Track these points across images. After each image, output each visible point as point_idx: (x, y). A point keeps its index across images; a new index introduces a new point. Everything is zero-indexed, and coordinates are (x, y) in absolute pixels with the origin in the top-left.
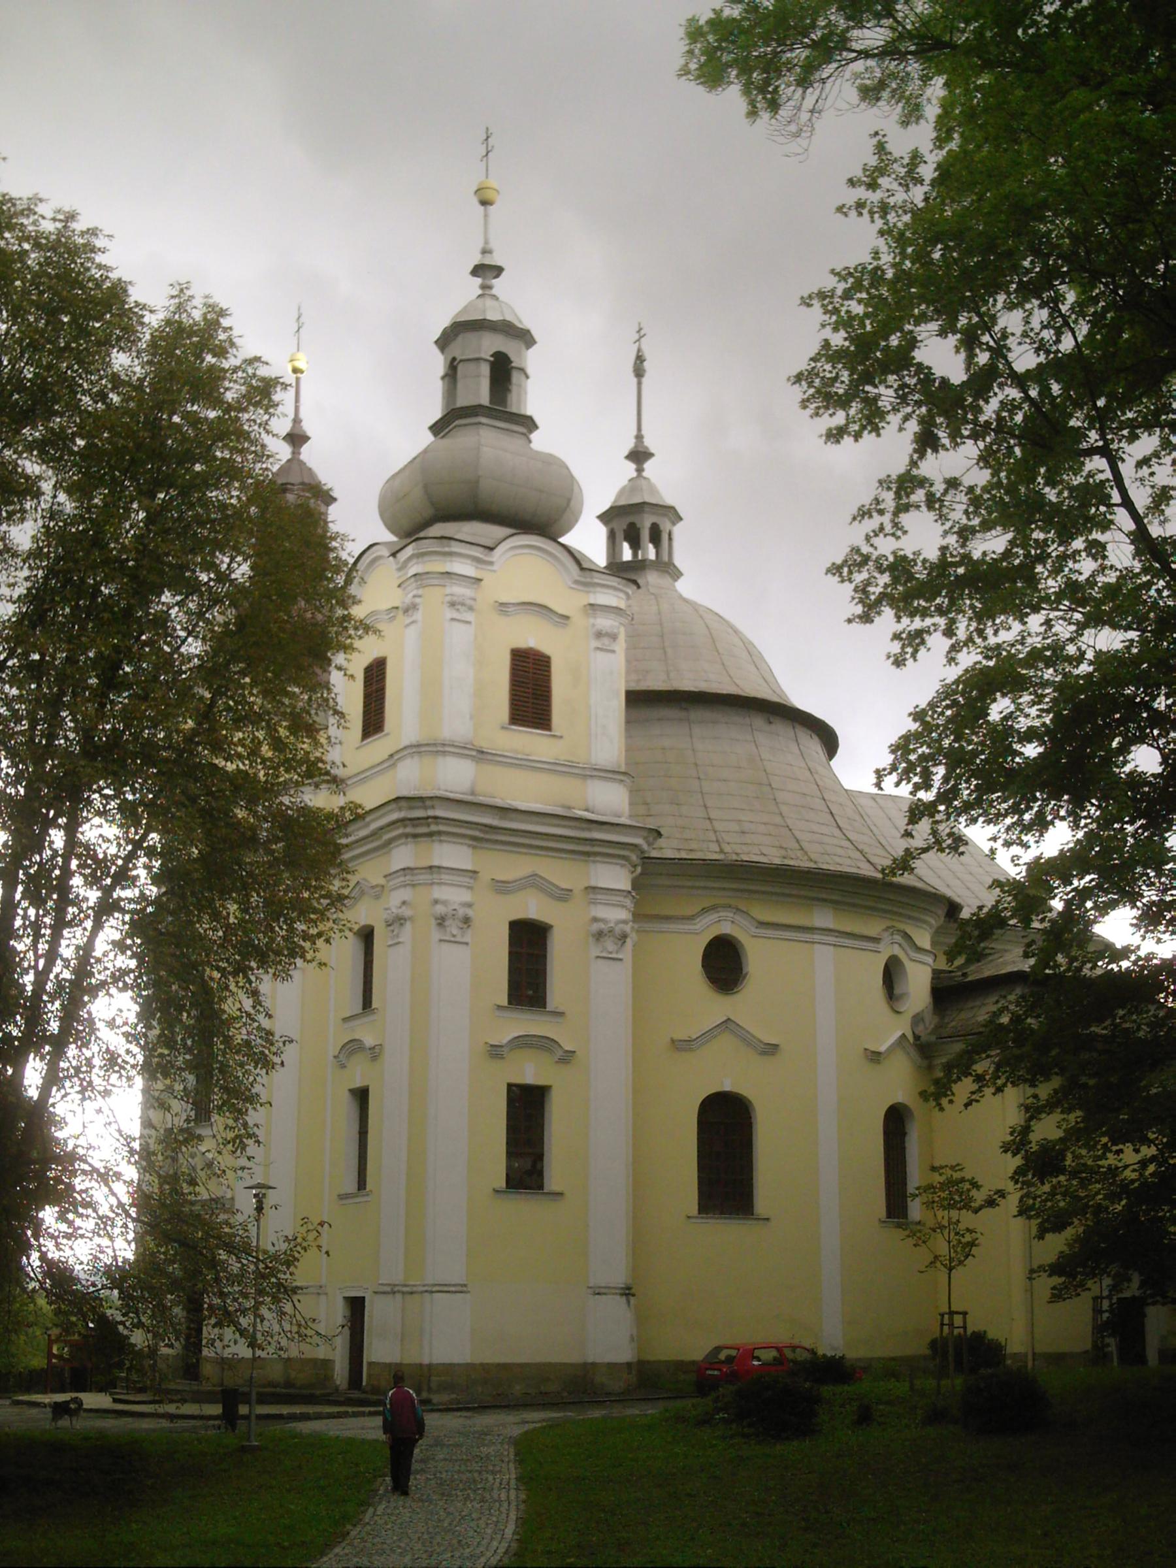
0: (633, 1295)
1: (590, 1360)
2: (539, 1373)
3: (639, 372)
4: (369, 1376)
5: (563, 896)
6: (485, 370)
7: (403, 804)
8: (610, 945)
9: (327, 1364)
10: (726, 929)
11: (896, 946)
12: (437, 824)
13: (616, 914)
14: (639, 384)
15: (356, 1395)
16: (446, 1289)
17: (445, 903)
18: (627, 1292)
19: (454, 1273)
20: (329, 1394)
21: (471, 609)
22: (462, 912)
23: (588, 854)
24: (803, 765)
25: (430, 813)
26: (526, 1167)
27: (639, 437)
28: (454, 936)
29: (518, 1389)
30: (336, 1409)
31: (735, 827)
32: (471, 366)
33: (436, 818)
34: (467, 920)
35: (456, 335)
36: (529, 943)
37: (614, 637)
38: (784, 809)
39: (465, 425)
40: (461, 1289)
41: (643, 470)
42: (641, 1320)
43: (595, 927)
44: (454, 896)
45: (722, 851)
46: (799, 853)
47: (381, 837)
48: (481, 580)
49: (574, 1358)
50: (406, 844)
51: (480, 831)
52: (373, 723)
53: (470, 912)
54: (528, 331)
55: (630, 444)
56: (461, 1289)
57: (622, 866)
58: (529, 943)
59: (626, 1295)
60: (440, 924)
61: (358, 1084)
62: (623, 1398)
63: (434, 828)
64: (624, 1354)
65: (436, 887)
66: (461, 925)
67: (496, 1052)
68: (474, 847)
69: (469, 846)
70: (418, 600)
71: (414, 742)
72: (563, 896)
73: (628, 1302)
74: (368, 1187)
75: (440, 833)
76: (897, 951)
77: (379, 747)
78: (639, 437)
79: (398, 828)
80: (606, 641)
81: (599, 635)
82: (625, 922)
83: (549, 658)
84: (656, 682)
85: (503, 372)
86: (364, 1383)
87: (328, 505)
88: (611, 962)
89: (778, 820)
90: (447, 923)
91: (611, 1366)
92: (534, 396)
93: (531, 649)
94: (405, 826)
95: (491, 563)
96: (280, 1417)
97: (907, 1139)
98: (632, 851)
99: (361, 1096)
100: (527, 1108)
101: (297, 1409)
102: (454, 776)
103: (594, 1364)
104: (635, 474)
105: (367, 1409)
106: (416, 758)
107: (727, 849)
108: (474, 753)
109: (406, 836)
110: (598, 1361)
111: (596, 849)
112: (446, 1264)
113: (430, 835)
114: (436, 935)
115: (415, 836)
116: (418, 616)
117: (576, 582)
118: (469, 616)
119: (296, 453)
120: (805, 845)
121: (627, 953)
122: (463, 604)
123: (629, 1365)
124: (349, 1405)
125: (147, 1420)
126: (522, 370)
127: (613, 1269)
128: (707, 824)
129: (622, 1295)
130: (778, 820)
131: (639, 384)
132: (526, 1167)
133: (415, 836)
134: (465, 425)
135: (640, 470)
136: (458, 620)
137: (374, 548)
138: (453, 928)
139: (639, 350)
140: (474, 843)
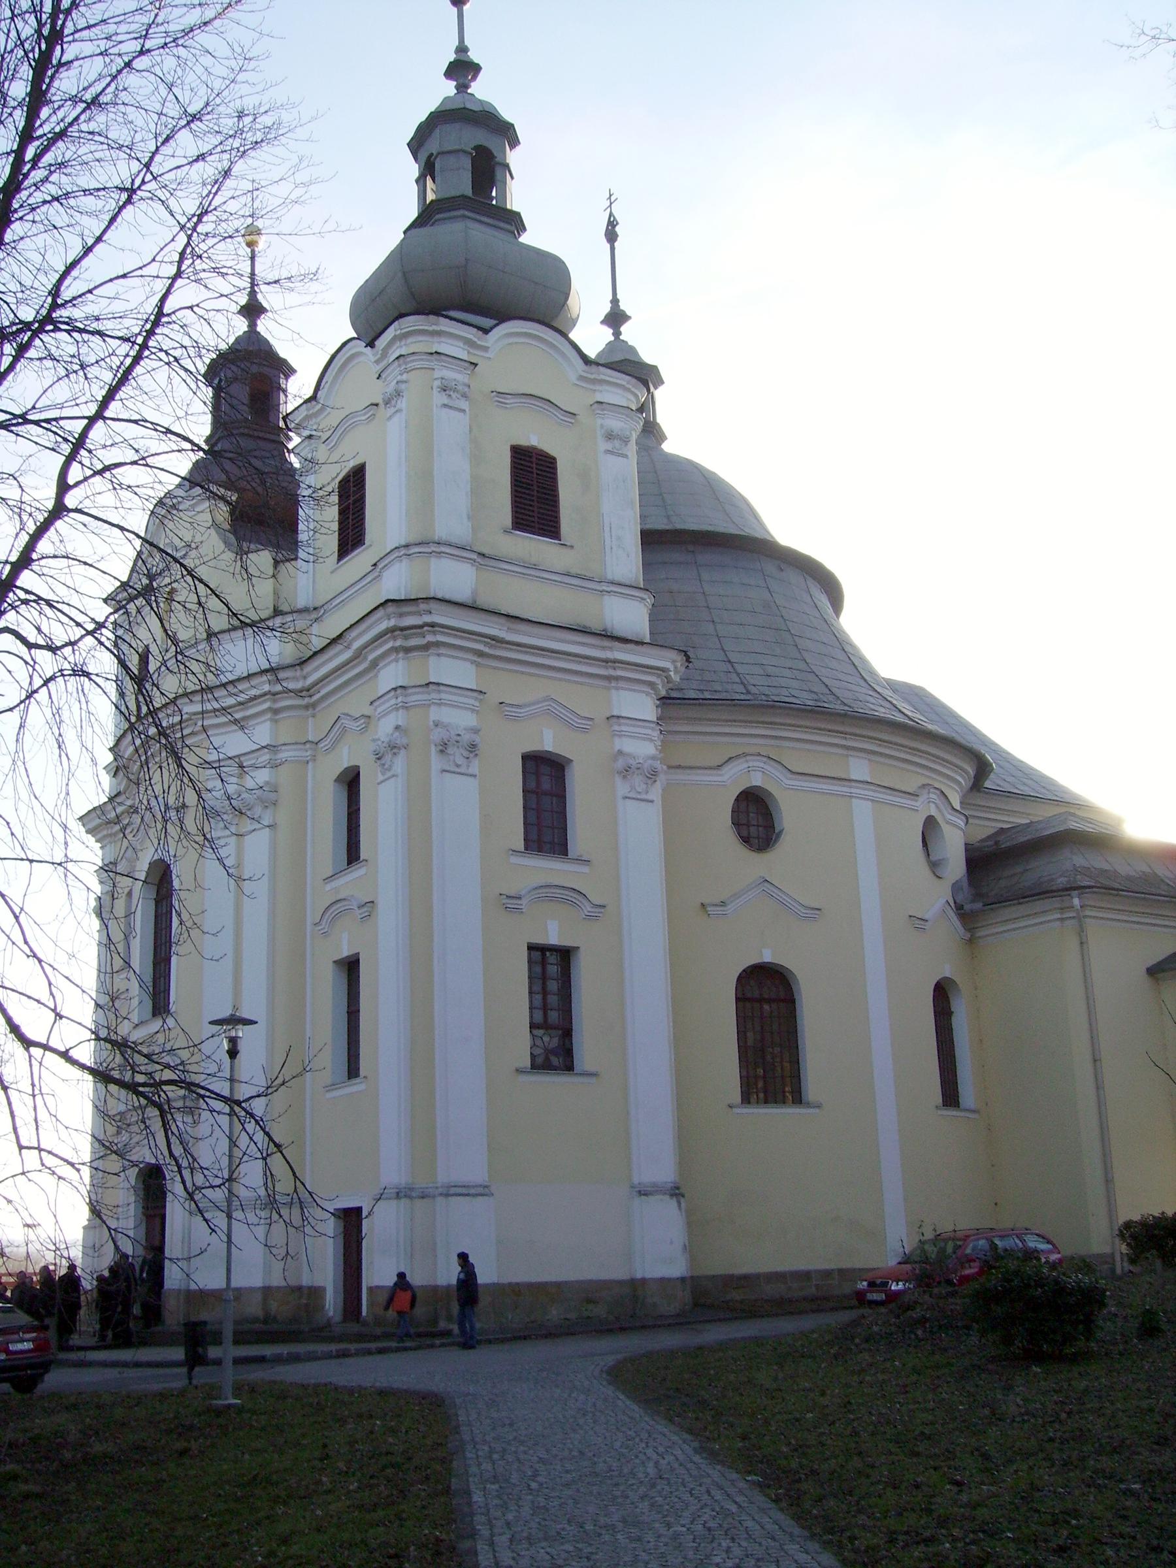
0: (683, 1196)
1: (639, 1275)
2: (590, 1292)
3: (611, 236)
4: (371, 1304)
5: (582, 725)
6: (467, 163)
7: (391, 609)
8: (638, 781)
9: (316, 1292)
10: (757, 780)
11: (932, 805)
12: (434, 633)
13: (643, 748)
14: (613, 249)
15: (354, 1328)
16: (464, 1191)
17: (446, 727)
18: (676, 1192)
19: (473, 1170)
20: (321, 1329)
21: (464, 396)
22: (467, 737)
23: (609, 678)
24: (818, 615)
25: (427, 619)
26: (555, 1043)
27: (615, 301)
28: (458, 766)
29: (555, 1314)
30: (333, 1347)
31: (757, 670)
32: (451, 160)
33: (432, 625)
34: (473, 747)
35: (431, 132)
36: (545, 777)
37: (626, 441)
38: (805, 655)
39: (445, 219)
40: (483, 1191)
41: (620, 333)
42: (695, 1225)
43: (620, 764)
44: (460, 719)
45: (748, 692)
46: (831, 698)
47: (365, 658)
48: (476, 365)
49: (619, 1273)
50: (397, 660)
51: (486, 644)
52: (351, 536)
53: (477, 739)
54: (513, 125)
55: (607, 308)
56: (483, 1191)
57: (647, 694)
58: (545, 777)
59: (676, 1195)
60: (442, 751)
61: (345, 952)
62: (679, 1322)
63: (430, 638)
64: (677, 1268)
65: (433, 709)
66: (466, 754)
67: (510, 903)
68: (478, 665)
69: (473, 662)
70: (403, 386)
71: (403, 543)
72: (582, 725)
73: (679, 1203)
74: (362, 1072)
75: (438, 644)
76: (933, 812)
77: (360, 560)
78: (615, 301)
79: (385, 642)
80: (617, 443)
81: (610, 436)
82: (653, 758)
83: (554, 459)
84: (660, 524)
85: (487, 170)
86: (364, 1313)
87: (287, 377)
88: (643, 804)
89: (802, 666)
90: (450, 751)
91: (663, 1281)
92: (519, 194)
93: (534, 448)
94: (395, 638)
95: (486, 349)
96: (262, 1360)
97: (954, 1019)
98: (659, 676)
99: (351, 967)
100: (552, 972)
101: (283, 1349)
102: (454, 578)
103: (644, 1281)
104: (612, 338)
105: (373, 1346)
106: (405, 561)
107: (753, 690)
108: (474, 556)
109: (395, 650)
110: (648, 1275)
111: (620, 673)
112: (465, 1161)
113: (426, 647)
114: (436, 762)
115: (407, 650)
116: (402, 404)
117: (581, 378)
118: (464, 404)
119: (252, 325)
120: (834, 690)
121: (656, 793)
122: (455, 390)
123: (683, 1280)
124: (351, 1342)
125: (91, 1370)
126: (507, 166)
127: (657, 1162)
128: (726, 667)
129: (672, 1195)
130: (802, 666)
131: (613, 249)
132: (555, 1043)
133: (407, 650)
134: (445, 219)
135: (617, 334)
136: (451, 407)
137: (350, 344)
138: (458, 754)
139: (611, 215)
140: (479, 660)
